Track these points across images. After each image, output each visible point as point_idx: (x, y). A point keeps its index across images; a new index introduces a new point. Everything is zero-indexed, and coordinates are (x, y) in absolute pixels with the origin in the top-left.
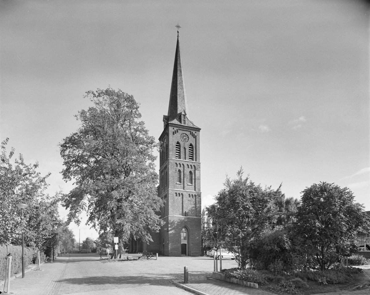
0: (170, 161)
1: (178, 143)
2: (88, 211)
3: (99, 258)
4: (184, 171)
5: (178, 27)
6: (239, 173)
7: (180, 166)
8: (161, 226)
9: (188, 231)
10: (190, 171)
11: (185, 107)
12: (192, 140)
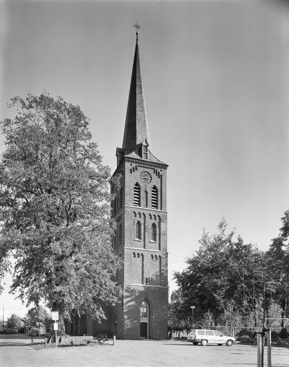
0: (127, 209)
1: (137, 184)
2: (14, 274)
3: (29, 341)
4: (145, 223)
5: (137, 27)
6: (221, 226)
7: (140, 217)
8: (118, 297)
9: (149, 306)
10: (152, 223)
11: (146, 137)
12: (156, 181)
